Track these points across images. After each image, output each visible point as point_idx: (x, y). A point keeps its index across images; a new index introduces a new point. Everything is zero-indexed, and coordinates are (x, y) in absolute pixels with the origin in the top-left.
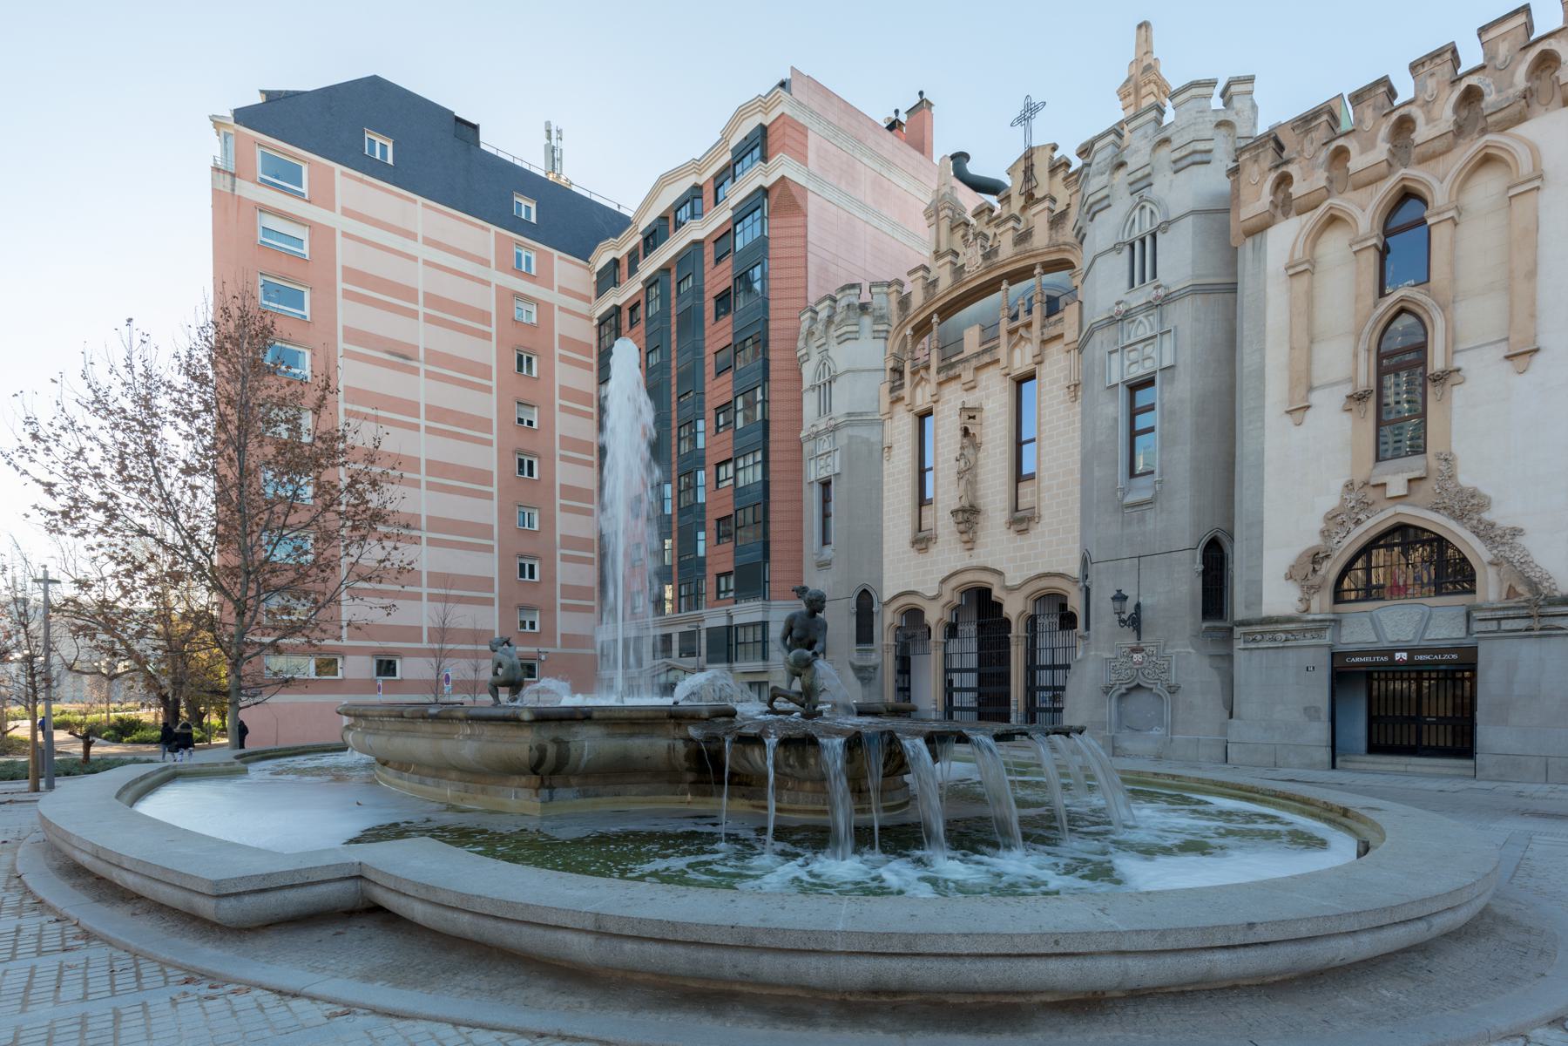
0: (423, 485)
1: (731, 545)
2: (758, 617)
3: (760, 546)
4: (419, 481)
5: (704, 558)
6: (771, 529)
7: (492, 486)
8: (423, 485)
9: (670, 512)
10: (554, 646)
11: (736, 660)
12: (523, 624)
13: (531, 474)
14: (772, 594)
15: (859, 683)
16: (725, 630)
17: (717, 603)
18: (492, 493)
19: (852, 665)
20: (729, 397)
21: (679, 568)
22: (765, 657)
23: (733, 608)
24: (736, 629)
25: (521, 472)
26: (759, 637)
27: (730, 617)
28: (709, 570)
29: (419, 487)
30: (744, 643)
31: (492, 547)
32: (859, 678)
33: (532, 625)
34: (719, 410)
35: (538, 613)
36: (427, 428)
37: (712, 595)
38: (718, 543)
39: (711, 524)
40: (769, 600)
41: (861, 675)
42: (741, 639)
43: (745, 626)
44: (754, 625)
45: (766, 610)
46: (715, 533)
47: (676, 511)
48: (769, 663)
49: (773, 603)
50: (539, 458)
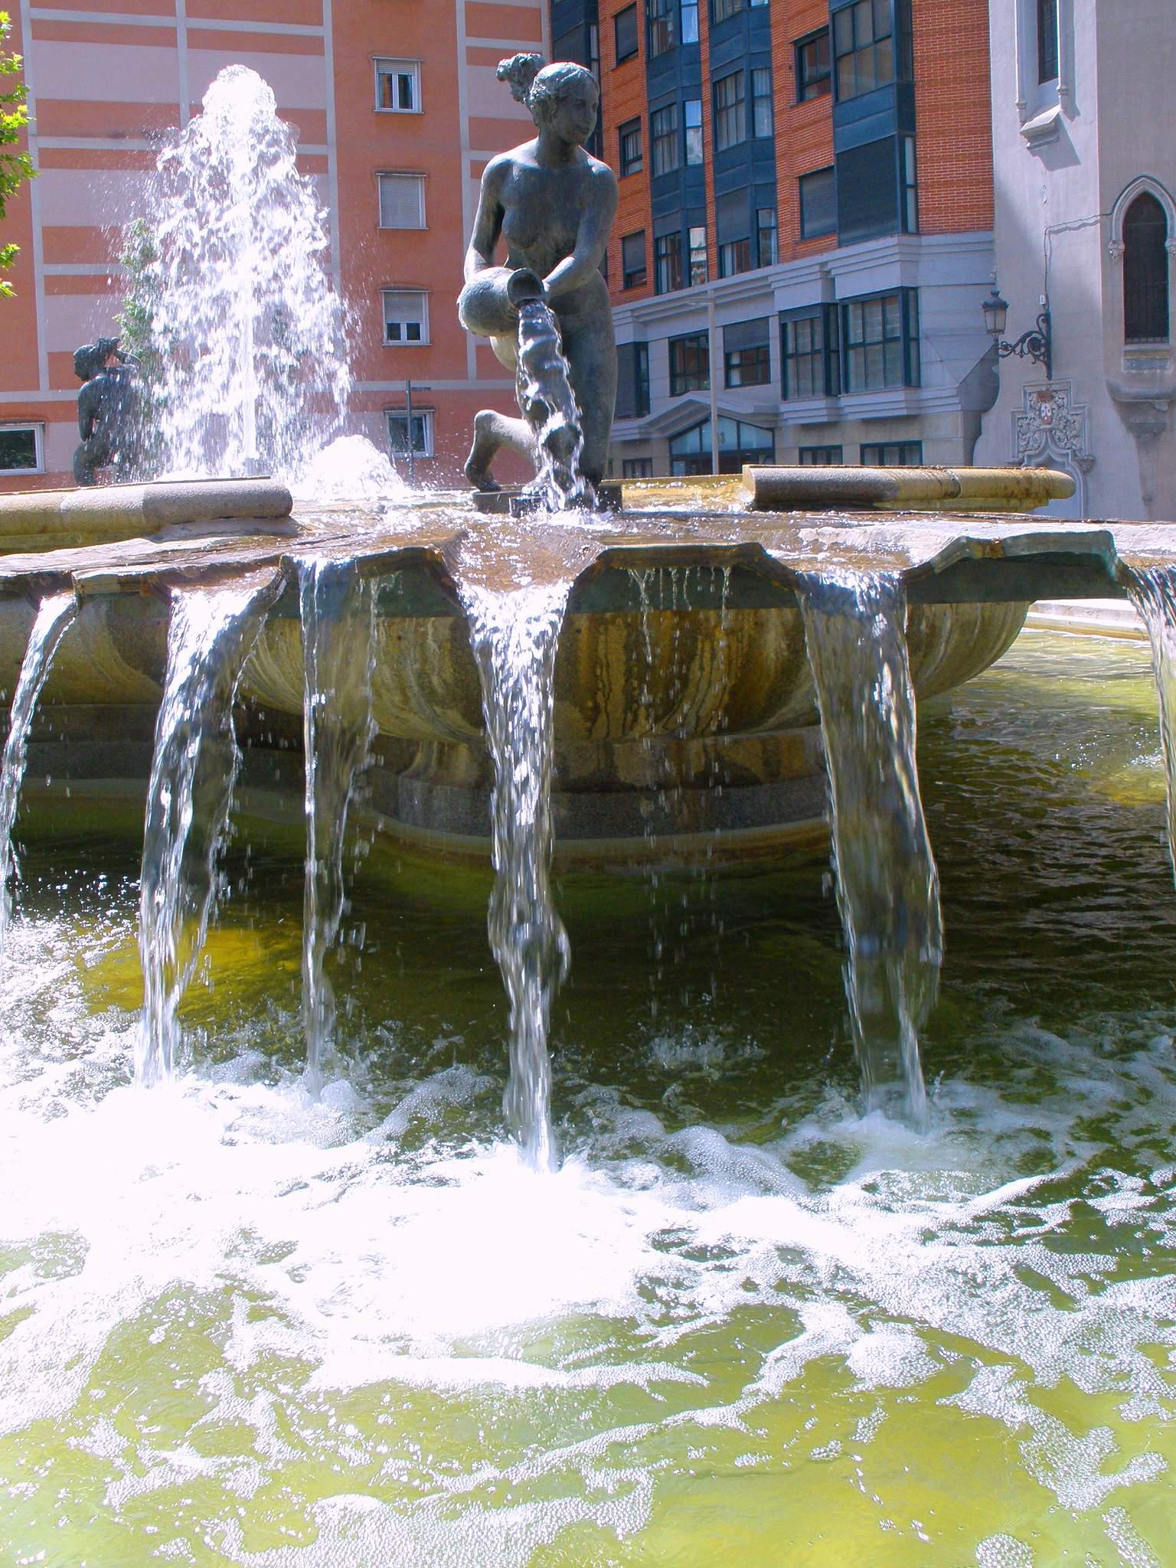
0: (182, 38)
1: (828, 100)
2: (889, 279)
3: (890, 99)
4: (173, 31)
5: (771, 140)
6: (917, 54)
7: (320, 23)
8: (182, 38)
9: (699, 162)
10: (463, 374)
11: (847, 391)
12: (394, 331)
13: (406, 101)
14: (923, 218)
15: (1131, 441)
16: (818, 313)
17: (801, 248)
18: (320, 40)
19: (1113, 391)
20: (824, 19)
21: (717, 171)
22: (911, 379)
23: (836, 256)
24: (845, 308)
25: (387, 100)
26: (896, 326)
27: (830, 282)
28: (782, 169)
29: (174, 44)
30: (863, 345)
31: (325, 158)
32: (1131, 428)
33: (414, 331)
34: (803, 46)
35: (425, 302)
36: (192, 33)
37: (788, 233)
38: (801, 99)
39: (783, 56)
40: (918, 233)
41: (1138, 419)
42: (855, 337)
43: (863, 301)
44: (883, 298)
45: (909, 261)
46: (792, 76)
47: (710, 158)
48: (926, 394)
49: (925, 240)
50: (428, 179)
